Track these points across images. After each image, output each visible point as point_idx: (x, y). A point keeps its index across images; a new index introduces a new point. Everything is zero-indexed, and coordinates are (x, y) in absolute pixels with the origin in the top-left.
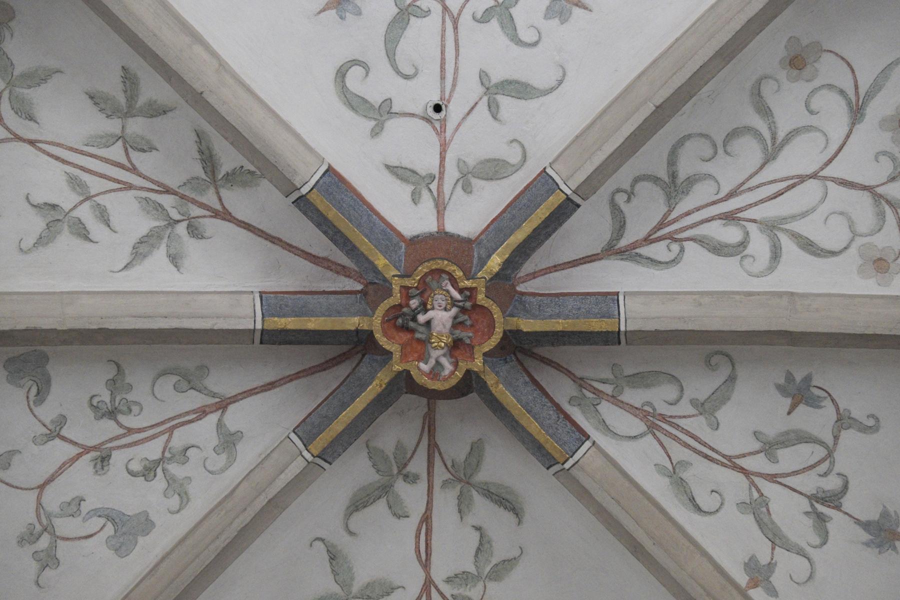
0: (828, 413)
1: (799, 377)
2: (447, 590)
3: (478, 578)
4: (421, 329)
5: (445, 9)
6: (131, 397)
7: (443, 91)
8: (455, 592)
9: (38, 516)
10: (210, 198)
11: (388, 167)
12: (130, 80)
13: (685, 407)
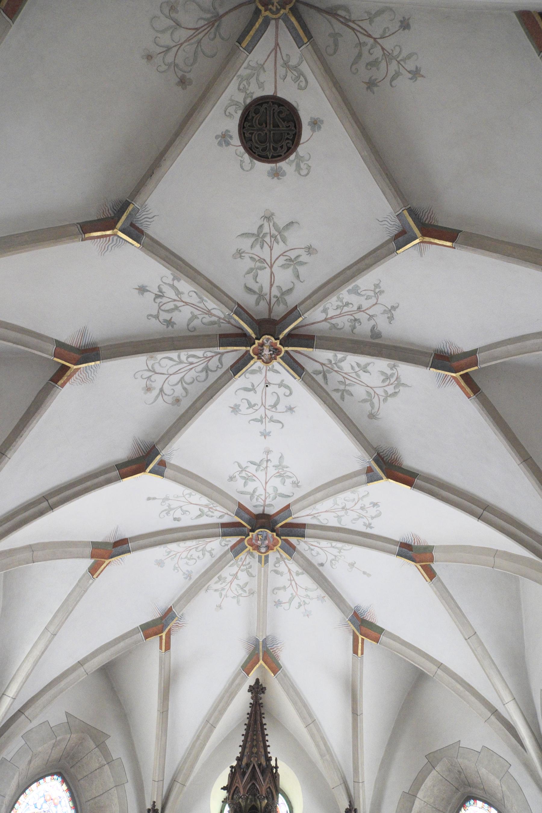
0: (161, 318)
1: (170, 327)
2: (266, 265)
3: (257, 269)
4: (271, 349)
5: (265, 407)
6: (350, 324)
7: (266, 389)
8: (264, 265)
9: (378, 297)
10: (325, 368)
11: (280, 373)
12: (342, 398)
13: (200, 317)
